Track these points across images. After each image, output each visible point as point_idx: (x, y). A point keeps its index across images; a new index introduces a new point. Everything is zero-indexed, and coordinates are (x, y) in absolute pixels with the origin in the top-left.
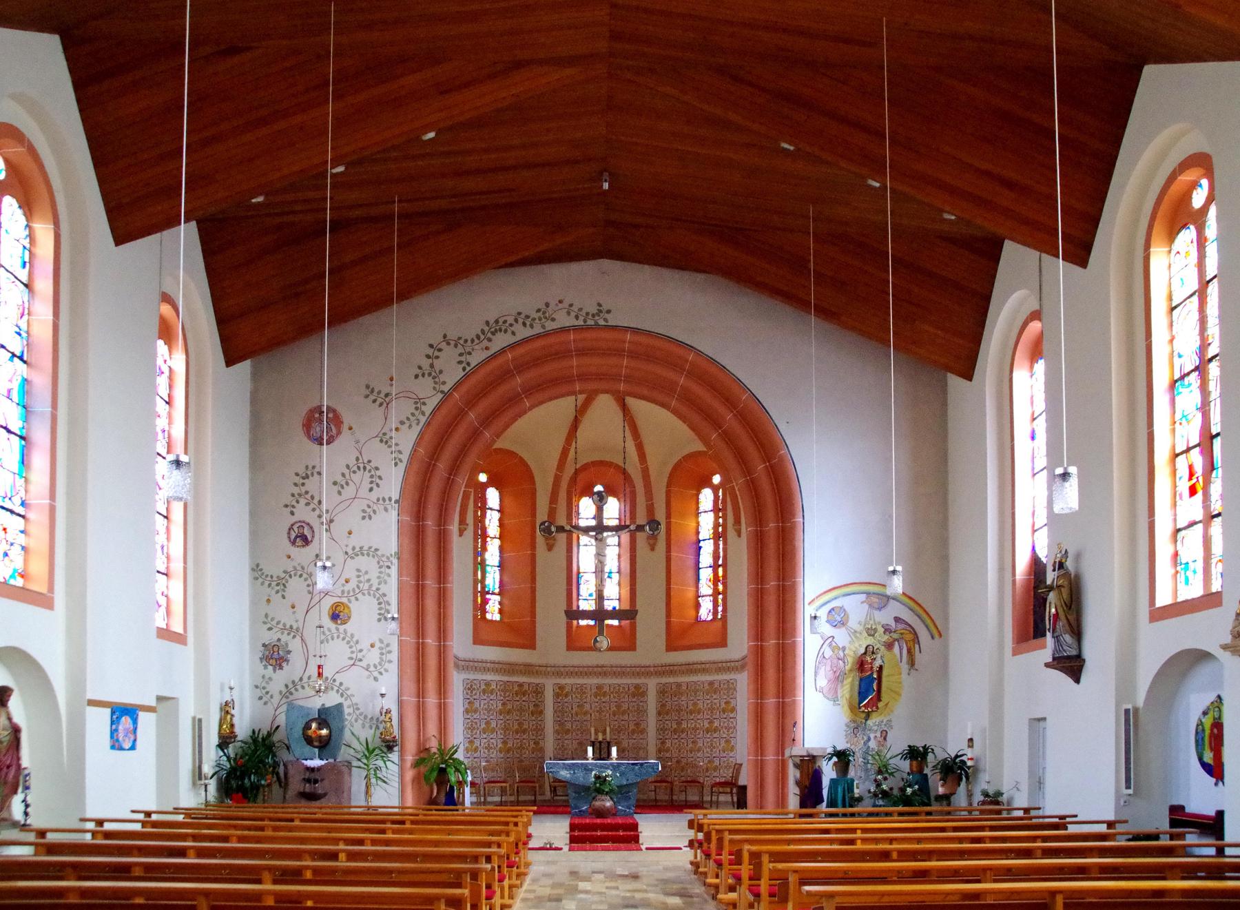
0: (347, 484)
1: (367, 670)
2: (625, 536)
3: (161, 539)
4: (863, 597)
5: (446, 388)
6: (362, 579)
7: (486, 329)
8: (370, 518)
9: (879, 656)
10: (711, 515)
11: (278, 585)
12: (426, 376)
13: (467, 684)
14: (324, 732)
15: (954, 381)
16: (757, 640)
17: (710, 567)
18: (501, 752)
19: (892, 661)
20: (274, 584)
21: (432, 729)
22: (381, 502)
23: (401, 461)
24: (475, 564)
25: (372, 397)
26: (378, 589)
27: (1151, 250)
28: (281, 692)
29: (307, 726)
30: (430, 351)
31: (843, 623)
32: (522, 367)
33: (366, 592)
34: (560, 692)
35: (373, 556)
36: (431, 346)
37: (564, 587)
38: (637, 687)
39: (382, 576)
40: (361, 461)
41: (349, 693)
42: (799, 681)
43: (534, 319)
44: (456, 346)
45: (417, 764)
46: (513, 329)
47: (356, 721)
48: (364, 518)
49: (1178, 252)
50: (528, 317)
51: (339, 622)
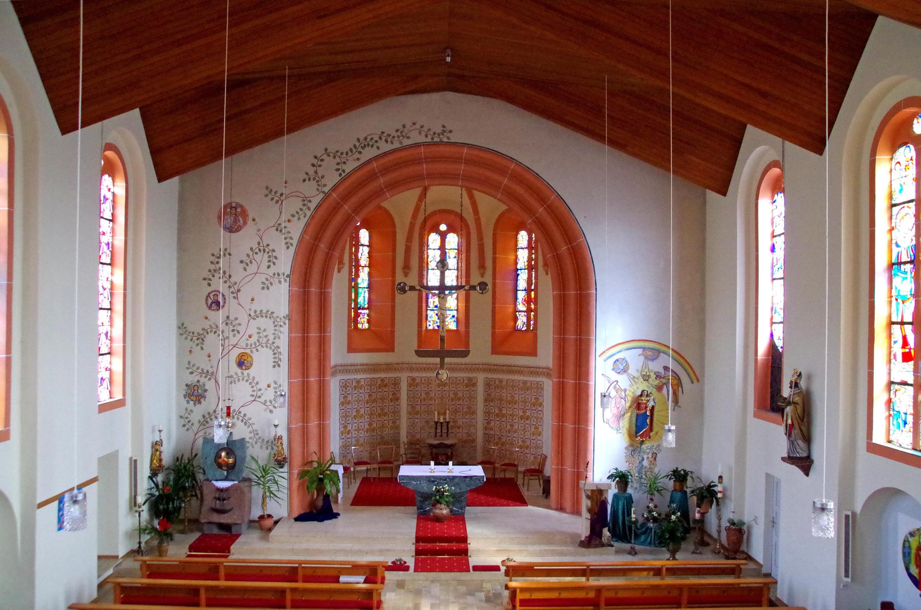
0: (251, 262)
1: (264, 404)
2: (463, 292)
3: (106, 328)
4: (640, 351)
5: (326, 189)
6: (261, 335)
7: (358, 144)
8: (268, 288)
9: (652, 398)
10: (526, 251)
11: (198, 339)
12: (312, 180)
13: (343, 383)
14: (231, 461)
15: (711, 195)
16: (560, 378)
17: (525, 290)
18: (367, 432)
19: (662, 402)
20: (195, 338)
21: (313, 446)
22: (276, 276)
23: (292, 245)
24: (350, 287)
25: (270, 196)
26: (273, 343)
27: (877, 157)
28: (199, 421)
29: (218, 456)
30: (315, 161)
31: (625, 370)
32: (385, 170)
33: (264, 345)
34: (412, 383)
35: (270, 318)
36: (316, 157)
37: (416, 305)
38: (470, 379)
39: (276, 333)
40: (261, 244)
41: (251, 422)
42: (591, 415)
43: (394, 137)
44: (334, 157)
45: (302, 474)
46: (378, 144)
47: (256, 443)
48: (263, 288)
49: (899, 163)
50: (389, 135)
51: (244, 368)
